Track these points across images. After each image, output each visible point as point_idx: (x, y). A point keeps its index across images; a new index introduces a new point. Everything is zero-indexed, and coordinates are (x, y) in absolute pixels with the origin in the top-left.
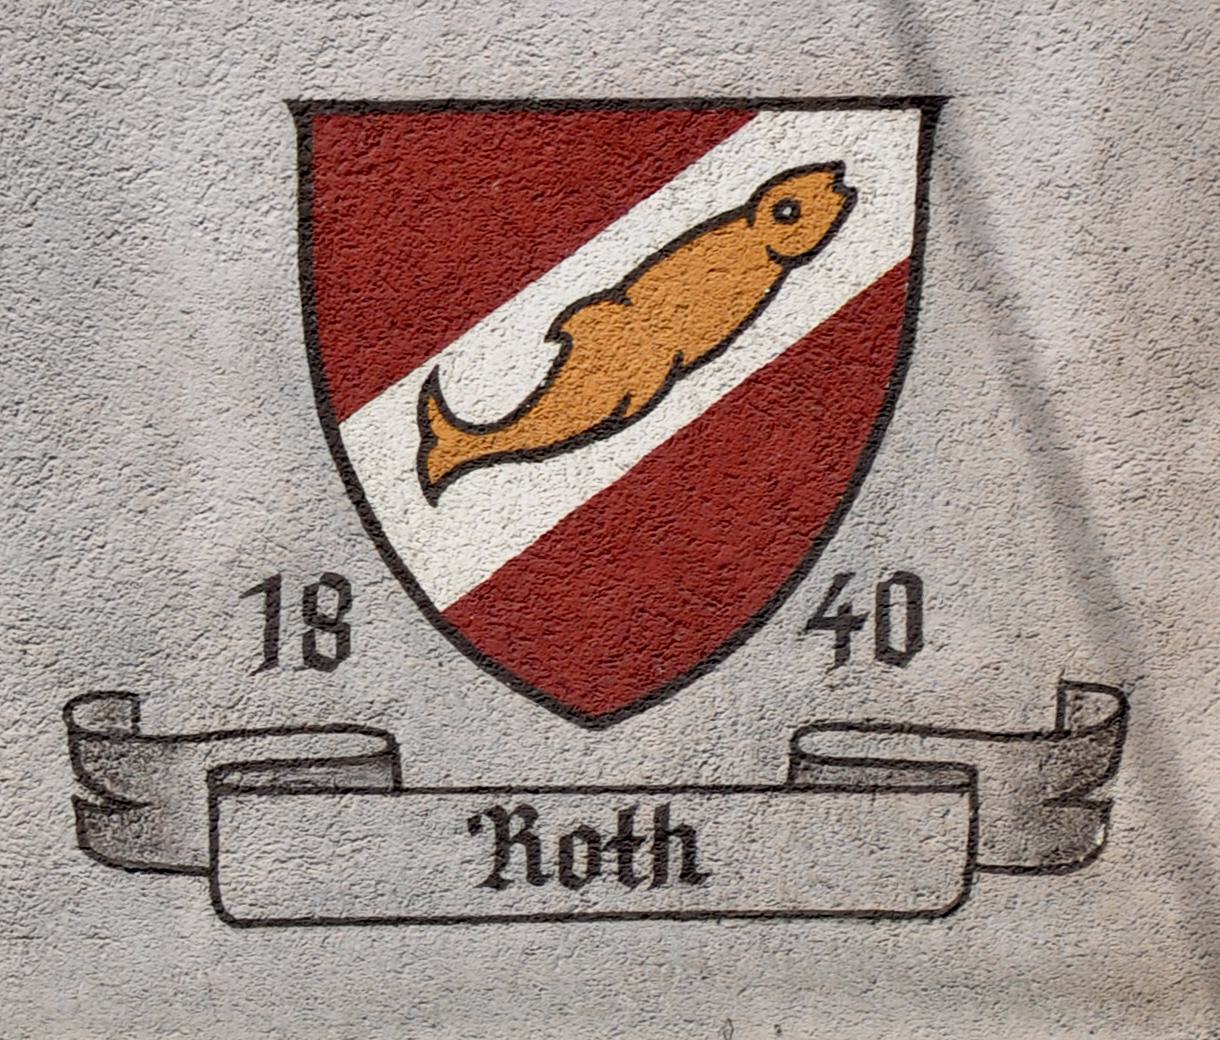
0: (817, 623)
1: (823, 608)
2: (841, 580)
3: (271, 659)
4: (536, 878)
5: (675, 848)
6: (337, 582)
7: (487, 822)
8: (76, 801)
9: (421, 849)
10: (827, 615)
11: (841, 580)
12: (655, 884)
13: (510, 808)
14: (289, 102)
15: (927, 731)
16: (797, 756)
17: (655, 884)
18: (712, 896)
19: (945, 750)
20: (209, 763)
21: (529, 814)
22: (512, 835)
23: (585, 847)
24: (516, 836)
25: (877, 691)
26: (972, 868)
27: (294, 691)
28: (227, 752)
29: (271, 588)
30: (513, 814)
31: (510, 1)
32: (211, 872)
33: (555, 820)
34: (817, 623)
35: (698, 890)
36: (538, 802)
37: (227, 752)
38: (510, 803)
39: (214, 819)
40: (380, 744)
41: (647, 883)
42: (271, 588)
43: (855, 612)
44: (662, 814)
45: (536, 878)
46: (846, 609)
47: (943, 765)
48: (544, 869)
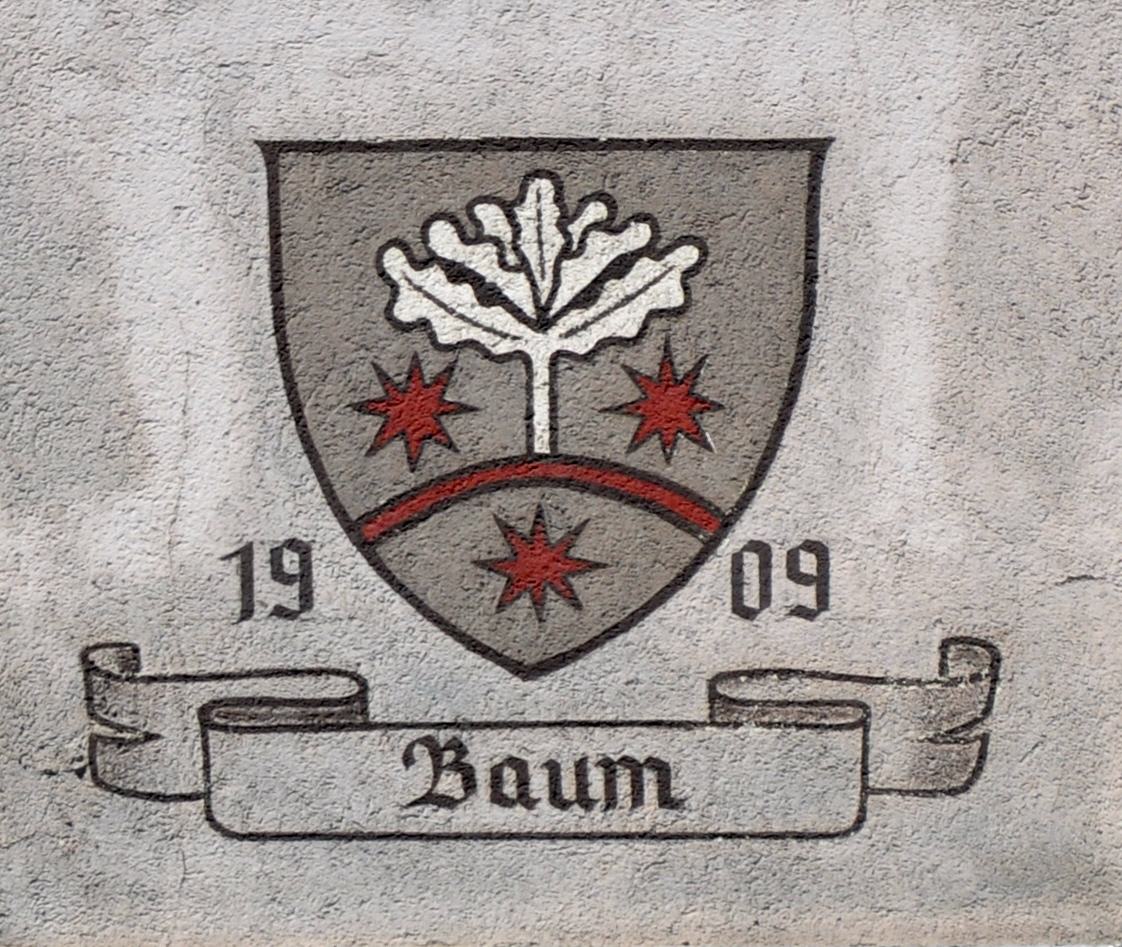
6: (303, 549)
9: (365, 775)
12: (608, 807)
15: (785, 673)
16: (713, 697)
17: (608, 807)
18: (689, 821)
19: (850, 691)
20: (775, 548)
21: (460, 749)
23: (514, 773)
24: (448, 764)
25: (778, 637)
27: (264, 643)
28: (221, 689)
29: (245, 554)
33: (484, 751)
35: (672, 814)
37: (221, 689)
38: (443, 737)
39: (205, 748)
41: (602, 803)
42: (245, 554)
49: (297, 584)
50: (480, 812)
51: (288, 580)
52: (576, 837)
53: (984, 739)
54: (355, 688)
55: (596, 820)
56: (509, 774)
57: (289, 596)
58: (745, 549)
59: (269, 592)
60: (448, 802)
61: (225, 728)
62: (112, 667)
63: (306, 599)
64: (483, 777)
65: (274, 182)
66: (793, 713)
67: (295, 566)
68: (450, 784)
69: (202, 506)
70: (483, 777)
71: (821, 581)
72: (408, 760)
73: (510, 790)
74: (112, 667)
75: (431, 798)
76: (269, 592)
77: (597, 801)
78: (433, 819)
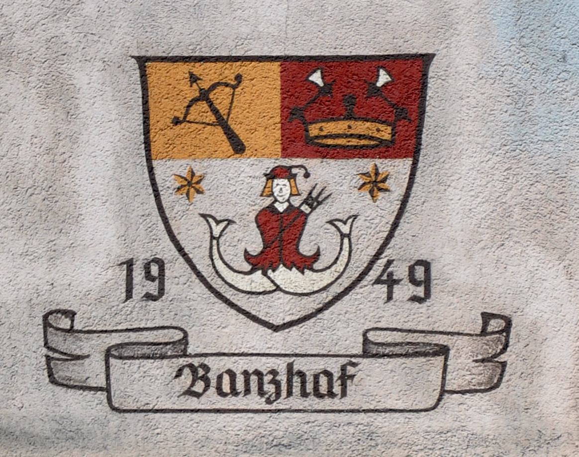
0: (378, 281)
1: (381, 275)
2: (389, 263)
3: (129, 294)
4: (304, 394)
5: (296, 381)
6: (161, 263)
7: (187, 371)
8: (47, 357)
10: (382, 278)
11: (389, 263)
13: (196, 364)
14: (433, 55)
16: (366, 341)
17: (342, 397)
22: (199, 375)
24: (200, 377)
26: (443, 392)
29: (130, 264)
30: (198, 367)
31: (297, 0)
32: (107, 389)
34: (378, 281)
36: (207, 361)
40: (178, 335)
41: (339, 396)
43: (395, 277)
44: (290, 367)
45: (304, 394)
46: (391, 275)
47: (418, 344)
48: (308, 391)
49: (423, 285)
50: (211, 399)
51: (153, 279)
52: (411, 411)
53: (504, 365)
54: (181, 335)
55: (327, 403)
56: (226, 379)
57: (153, 288)
58: (153, 261)
59: (142, 286)
60: (198, 395)
61: (120, 358)
62: (57, 322)
63: (428, 294)
64: (214, 383)
65: (144, 76)
66: (146, 350)
67: (156, 271)
68: (199, 387)
69: (572, 253)
70: (214, 383)
71: (427, 283)
72: (179, 373)
73: (226, 388)
74: (57, 322)
75: (190, 392)
76: (142, 286)
77: (338, 395)
78: (193, 403)
